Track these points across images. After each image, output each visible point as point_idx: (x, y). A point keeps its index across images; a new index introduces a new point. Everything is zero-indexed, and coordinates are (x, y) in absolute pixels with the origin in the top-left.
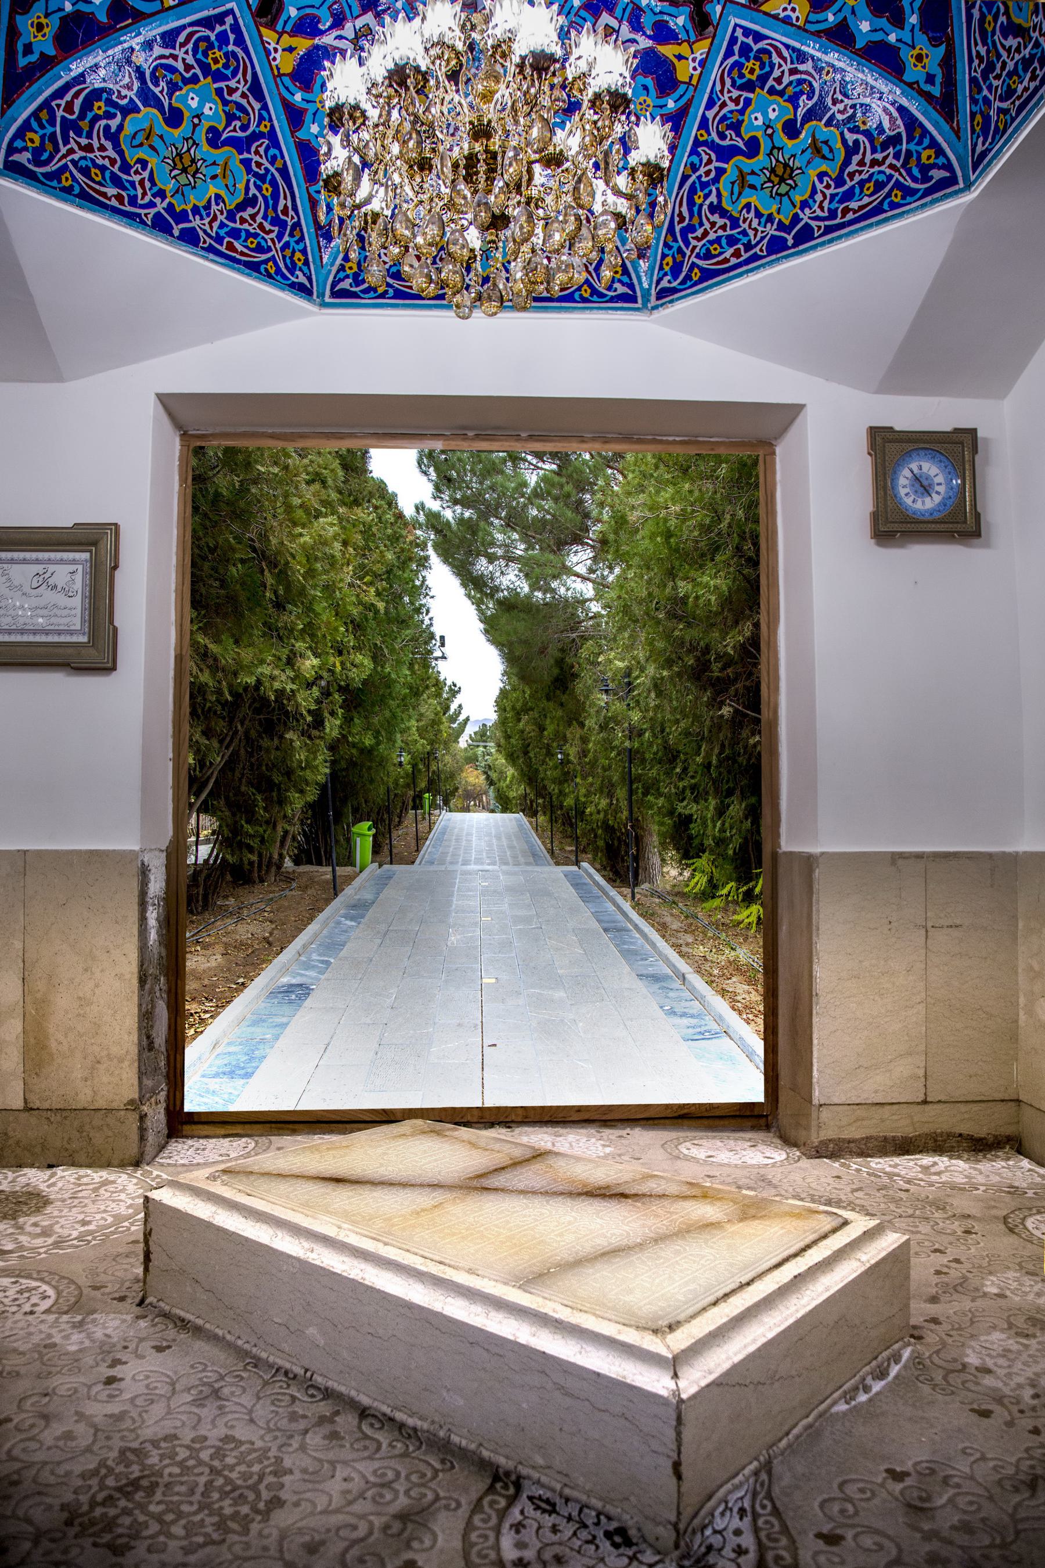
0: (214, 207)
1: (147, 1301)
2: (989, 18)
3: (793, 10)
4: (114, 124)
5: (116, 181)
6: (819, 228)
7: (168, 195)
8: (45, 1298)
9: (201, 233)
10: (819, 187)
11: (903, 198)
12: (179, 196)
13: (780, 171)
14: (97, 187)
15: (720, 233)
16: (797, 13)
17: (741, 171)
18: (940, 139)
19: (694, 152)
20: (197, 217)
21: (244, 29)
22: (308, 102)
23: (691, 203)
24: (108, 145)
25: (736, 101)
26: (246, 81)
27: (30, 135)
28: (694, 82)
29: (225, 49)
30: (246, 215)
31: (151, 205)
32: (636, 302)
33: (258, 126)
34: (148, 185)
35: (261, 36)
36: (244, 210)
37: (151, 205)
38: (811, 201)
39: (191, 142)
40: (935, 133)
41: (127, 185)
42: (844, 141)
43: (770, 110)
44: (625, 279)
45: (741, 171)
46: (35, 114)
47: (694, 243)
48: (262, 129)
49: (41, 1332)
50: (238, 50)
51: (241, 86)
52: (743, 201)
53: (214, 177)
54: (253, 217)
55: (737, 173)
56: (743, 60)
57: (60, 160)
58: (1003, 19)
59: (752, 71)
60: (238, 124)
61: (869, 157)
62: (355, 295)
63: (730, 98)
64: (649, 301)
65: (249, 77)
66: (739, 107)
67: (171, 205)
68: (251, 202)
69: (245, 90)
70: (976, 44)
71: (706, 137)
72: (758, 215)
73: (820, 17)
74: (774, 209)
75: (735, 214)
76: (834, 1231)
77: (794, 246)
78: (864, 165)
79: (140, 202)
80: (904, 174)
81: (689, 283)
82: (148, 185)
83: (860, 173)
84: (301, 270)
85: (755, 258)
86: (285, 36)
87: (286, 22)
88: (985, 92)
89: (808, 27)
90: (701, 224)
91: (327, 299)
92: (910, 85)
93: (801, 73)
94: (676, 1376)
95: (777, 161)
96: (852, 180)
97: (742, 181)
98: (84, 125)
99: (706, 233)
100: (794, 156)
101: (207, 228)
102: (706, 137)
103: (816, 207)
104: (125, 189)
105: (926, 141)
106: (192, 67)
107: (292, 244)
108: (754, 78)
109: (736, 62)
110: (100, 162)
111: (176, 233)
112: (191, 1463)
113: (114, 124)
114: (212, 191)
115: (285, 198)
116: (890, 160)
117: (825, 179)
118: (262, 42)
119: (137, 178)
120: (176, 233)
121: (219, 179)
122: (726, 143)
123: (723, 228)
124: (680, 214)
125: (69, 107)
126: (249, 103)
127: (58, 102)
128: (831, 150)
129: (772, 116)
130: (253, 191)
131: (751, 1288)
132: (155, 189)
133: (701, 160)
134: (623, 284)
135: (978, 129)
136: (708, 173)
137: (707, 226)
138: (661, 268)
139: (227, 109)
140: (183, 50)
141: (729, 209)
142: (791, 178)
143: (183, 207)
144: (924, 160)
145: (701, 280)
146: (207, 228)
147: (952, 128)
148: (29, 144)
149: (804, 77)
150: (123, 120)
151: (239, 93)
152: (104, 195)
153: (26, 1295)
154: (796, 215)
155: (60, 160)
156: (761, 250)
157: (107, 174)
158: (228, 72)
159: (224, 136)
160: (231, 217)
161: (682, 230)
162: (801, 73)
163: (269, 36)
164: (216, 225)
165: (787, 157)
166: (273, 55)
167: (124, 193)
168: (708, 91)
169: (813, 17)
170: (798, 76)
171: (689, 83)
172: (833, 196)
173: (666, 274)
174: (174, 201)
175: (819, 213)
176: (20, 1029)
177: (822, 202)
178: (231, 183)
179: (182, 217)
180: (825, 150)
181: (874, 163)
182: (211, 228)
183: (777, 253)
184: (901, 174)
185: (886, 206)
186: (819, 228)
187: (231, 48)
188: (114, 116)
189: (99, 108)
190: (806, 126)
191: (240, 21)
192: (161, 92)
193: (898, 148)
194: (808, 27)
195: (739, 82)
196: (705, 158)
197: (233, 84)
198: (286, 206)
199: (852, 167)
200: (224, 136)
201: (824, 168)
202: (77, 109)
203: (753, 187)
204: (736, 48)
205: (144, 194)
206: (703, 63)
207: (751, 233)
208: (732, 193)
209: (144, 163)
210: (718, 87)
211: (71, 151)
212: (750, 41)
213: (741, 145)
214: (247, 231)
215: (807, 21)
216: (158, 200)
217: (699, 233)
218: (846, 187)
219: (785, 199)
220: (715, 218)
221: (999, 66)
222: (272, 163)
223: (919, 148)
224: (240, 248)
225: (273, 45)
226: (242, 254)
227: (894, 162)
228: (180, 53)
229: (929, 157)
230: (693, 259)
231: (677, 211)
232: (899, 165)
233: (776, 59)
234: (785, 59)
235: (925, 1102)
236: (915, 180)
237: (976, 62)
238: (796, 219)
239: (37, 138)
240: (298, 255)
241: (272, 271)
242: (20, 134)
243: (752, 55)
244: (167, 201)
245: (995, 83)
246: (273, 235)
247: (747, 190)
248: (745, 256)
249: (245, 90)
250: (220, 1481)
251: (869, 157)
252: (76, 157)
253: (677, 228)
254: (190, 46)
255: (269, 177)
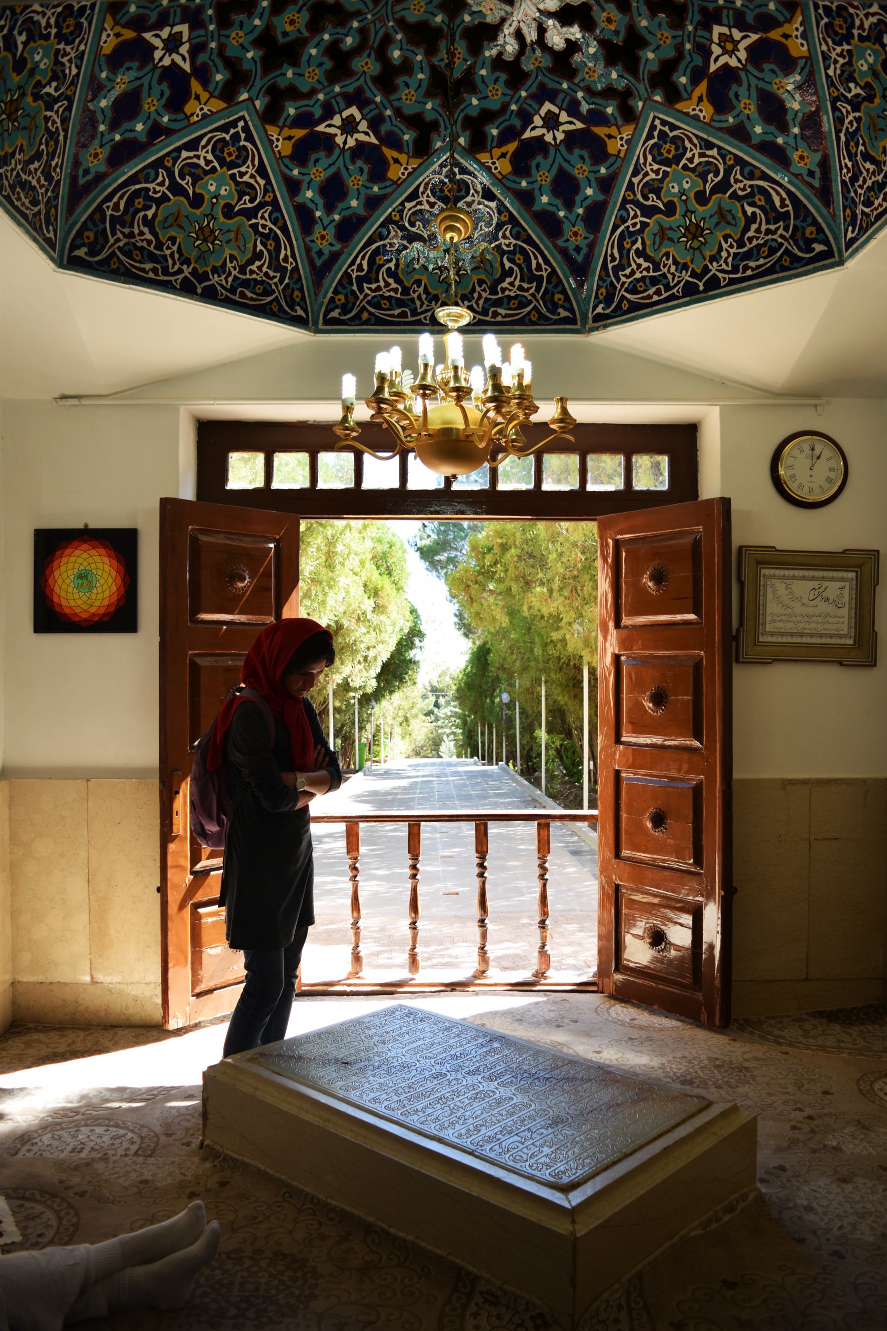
0: (229, 265)
1: (205, 1143)
2: (852, 144)
3: (701, 111)
4: (150, 213)
5: (153, 258)
6: (725, 279)
7: (193, 261)
8: (132, 1143)
9: (219, 288)
10: (725, 246)
11: (791, 263)
12: (201, 260)
13: (693, 230)
14: (137, 265)
15: (645, 273)
16: (704, 113)
17: (661, 226)
18: (820, 220)
19: (623, 207)
20: (216, 276)
21: (252, 128)
22: (303, 174)
23: (621, 248)
24: (146, 230)
25: (657, 172)
26: (254, 166)
27: (87, 233)
28: (622, 155)
29: (237, 145)
30: (254, 267)
31: (180, 271)
32: (576, 324)
33: (264, 197)
34: (177, 256)
35: (266, 132)
36: (253, 263)
37: (180, 271)
38: (718, 256)
39: (210, 217)
40: (816, 215)
41: (161, 259)
42: (744, 212)
43: (684, 182)
44: (567, 305)
45: (661, 226)
46: (91, 217)
47: (623, 279)
48: (267, 199)
49: (135, 1171)
50: (249, 145)
51: (250, 170)
52: (664, 251)
53: (228, 242)
54: (260, 268)
55: (658, 227)
56: (661, 142)
57: (109, 248)
58: (861, 148)
59: (669, 152)
60: (247, 198)
61: (764, 227)
62: (343, 323)
63: (652, 170)
64: (586, 323)
65: (256, 162)
66: (659, 177)
67: (195, 269)
68: (258, 256)
69: (253, 172)
70: (844, 158)
71: (632, 197)
72: (676, 262)
73: (723, 118)
74: (688, 260)
75: (657, 259)
76: (700, 1111)
77: (705, 291)
78: (760, 232)
79: (171, 270)
80: (792, 243)
81: (619, 312)
82: (177, 256)
83: (757, 238)
84: (299, 305)
85: (673, 297)
86: (286, 129)
87: (286, 119)
88: (852, 194)
89: (713, 124)
90: (630, 265)
91: (321, 326)
92: (796, 176)
93: (709, 156)
94: (573, 1222)
95: (691, 221)
96: (750, 243)
97: (663, 234)
98: (128, 218)
99: (633, 273)
100: (704, 219)
101: (224, 282)
102: (632, 197)
103: (722, 262)
104: (158, 262)
105: (809, 220)
106: (212, 162)
107: (292, 285)
108: (670, 156)
109: (655, 143)
110: (140, 244)
111: (199, 291)
112: (255, 1269)
113: (150, 213)
114: (227, 252)
115: (286, 249)
116: (781, 231)
117: (730, 240)
118: (267, 135)
119: (168, 252)
120: (199, 291)
121: (232, 243)
122: (650, 203)
123: (647, 269)
124: (612, 255)
125: (116, 207)
126: (256, 181)
127: (108, 204)
128: (734, 218)
129: (686, 186)
130: (260, 247)
131: (632, 1158)
132: (182, 259)
133: (629, 214)
134: (565, 309)
135: (848, 219)
136: (634, 225)
137: (634, 266)
138: (597, 297)
139: (238, 188)
140: (204, 150)
141: (652, 255)
142: (702, 236)
143: (205, 269)
144: (808, 235)
145: (629, 311)
146: (224, 282)
147: (829, 212)
148: (86, 241)
149: (710, 160)
150: (157, 209)
151: (248, 175)
152: (143, 270)
153: (118, 1141)
154: (706, 266)
155: (109, 248)
156: (678, 291)
157: (145, 253)
158: (240, 162)
159: (237, 209)
160: (242, 270)
161: (613, 267)
162: (709, 156)
163: (273, 131)
164: (230, 279)
165: (698, 219)
166: (276, 143)
167: (158, 266)
168: (634, 162)
169: (716, 117)
170: (706, 159)
171: (618, 156)
172: (735, 254)
173: (600, 302)
174: (197, 266)
175: (724, 266)
176: (86, 920)
177: (726, 259)
178: (241, 244)
179: (204, 277)
180: (729, 217)
181: (768, 231)
182: (227, 282)
183: (690, 295)
184: (789, 244)
185: (777, 268)
186: (725, 279)
187: (242, 143)
188: (150, 207)
189: (139, 203)
190: (714, 197)
191: (250, 124)
192: (187, 184)
193: (787, 222)
194: (713, 124)
195: (658, 158)
196: (632, 213)
197: (243, 169)
198: (286, 255)
199: (751, 234)
200: (237, 209)
201: (728, 231)
202: (122, 207)
203: (671, 240)
204: (656, 134)
205: (174, 264)
206: (628, 142)
207: (670, 277)
208: (654, 243)
209: (173, 239)
210: (642, 160)
211: (118, 240)
212: (666, 129)
213: (661, 206)
214: (255, 280)
215: (712, 120)
216: (185, 267)
217: (628, 271)
218: (745, 249)
219: (697, 252)
220: (641, 261)
221: (861, 179)
222: (275, 224)
223: (804, 225)
224: (249, 295)
225: (276, 136)
226: (252, 299)
227: (784, 233)
228: (202, 153)
229: (811, 233)
230: (623, 292)
231: (609, 252)
232: (787, 236)
233: (687, 144)
234: (695, 146)
235: (807, 979)
236: (800, 250)
237: (845, 171)
238: (706, 270)
239: (91, 235)
240: (296, 293)
241: (276, 310)
242: (79, 234)
243: (669, 139)
244: (192, 266)
245: (859, 191)
246: (276, 280)
247: (666, 242)
248: (665, 295)
249: (253, 172)
250: (276, 1282)
251: (764, 227)
252: (121, 244)
253: (610, 266)
254: (210, 147)
255: (272, 235)
